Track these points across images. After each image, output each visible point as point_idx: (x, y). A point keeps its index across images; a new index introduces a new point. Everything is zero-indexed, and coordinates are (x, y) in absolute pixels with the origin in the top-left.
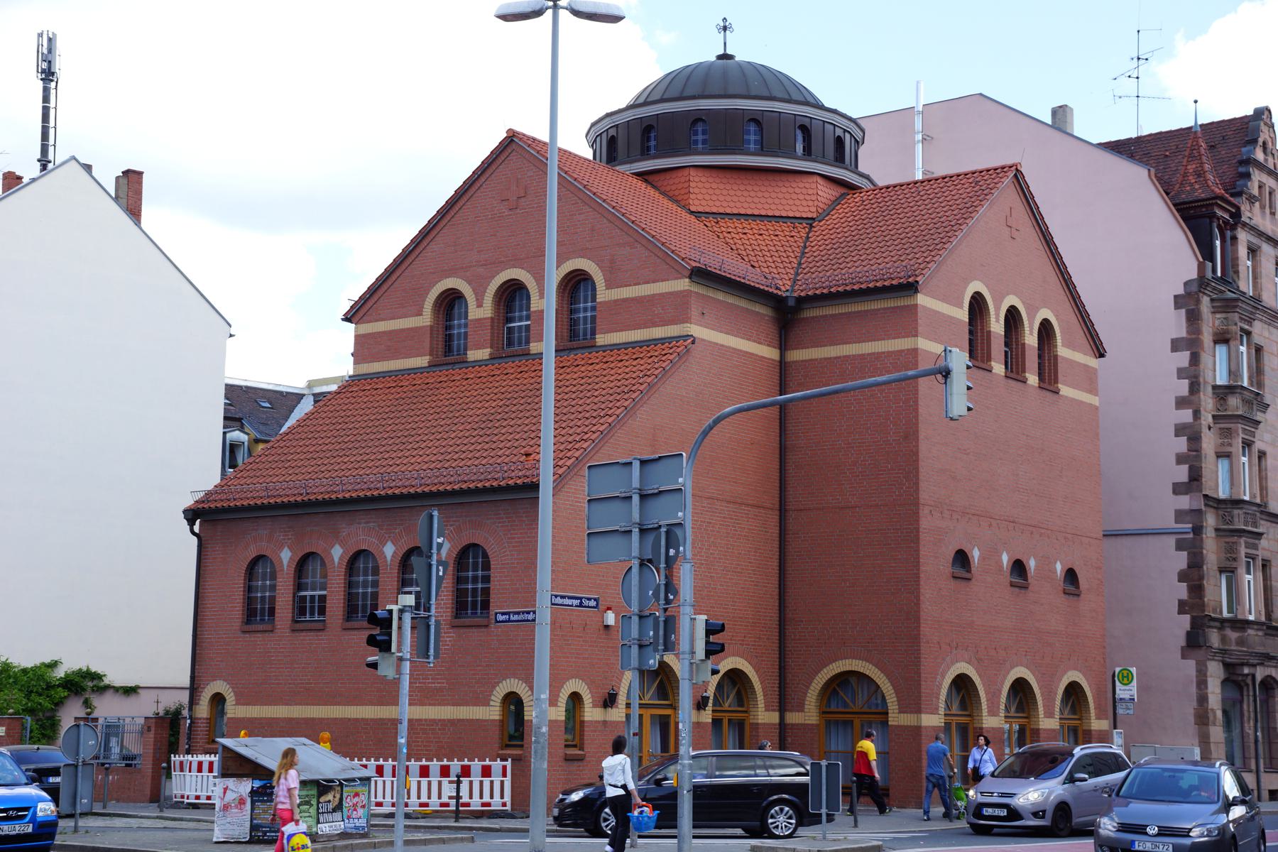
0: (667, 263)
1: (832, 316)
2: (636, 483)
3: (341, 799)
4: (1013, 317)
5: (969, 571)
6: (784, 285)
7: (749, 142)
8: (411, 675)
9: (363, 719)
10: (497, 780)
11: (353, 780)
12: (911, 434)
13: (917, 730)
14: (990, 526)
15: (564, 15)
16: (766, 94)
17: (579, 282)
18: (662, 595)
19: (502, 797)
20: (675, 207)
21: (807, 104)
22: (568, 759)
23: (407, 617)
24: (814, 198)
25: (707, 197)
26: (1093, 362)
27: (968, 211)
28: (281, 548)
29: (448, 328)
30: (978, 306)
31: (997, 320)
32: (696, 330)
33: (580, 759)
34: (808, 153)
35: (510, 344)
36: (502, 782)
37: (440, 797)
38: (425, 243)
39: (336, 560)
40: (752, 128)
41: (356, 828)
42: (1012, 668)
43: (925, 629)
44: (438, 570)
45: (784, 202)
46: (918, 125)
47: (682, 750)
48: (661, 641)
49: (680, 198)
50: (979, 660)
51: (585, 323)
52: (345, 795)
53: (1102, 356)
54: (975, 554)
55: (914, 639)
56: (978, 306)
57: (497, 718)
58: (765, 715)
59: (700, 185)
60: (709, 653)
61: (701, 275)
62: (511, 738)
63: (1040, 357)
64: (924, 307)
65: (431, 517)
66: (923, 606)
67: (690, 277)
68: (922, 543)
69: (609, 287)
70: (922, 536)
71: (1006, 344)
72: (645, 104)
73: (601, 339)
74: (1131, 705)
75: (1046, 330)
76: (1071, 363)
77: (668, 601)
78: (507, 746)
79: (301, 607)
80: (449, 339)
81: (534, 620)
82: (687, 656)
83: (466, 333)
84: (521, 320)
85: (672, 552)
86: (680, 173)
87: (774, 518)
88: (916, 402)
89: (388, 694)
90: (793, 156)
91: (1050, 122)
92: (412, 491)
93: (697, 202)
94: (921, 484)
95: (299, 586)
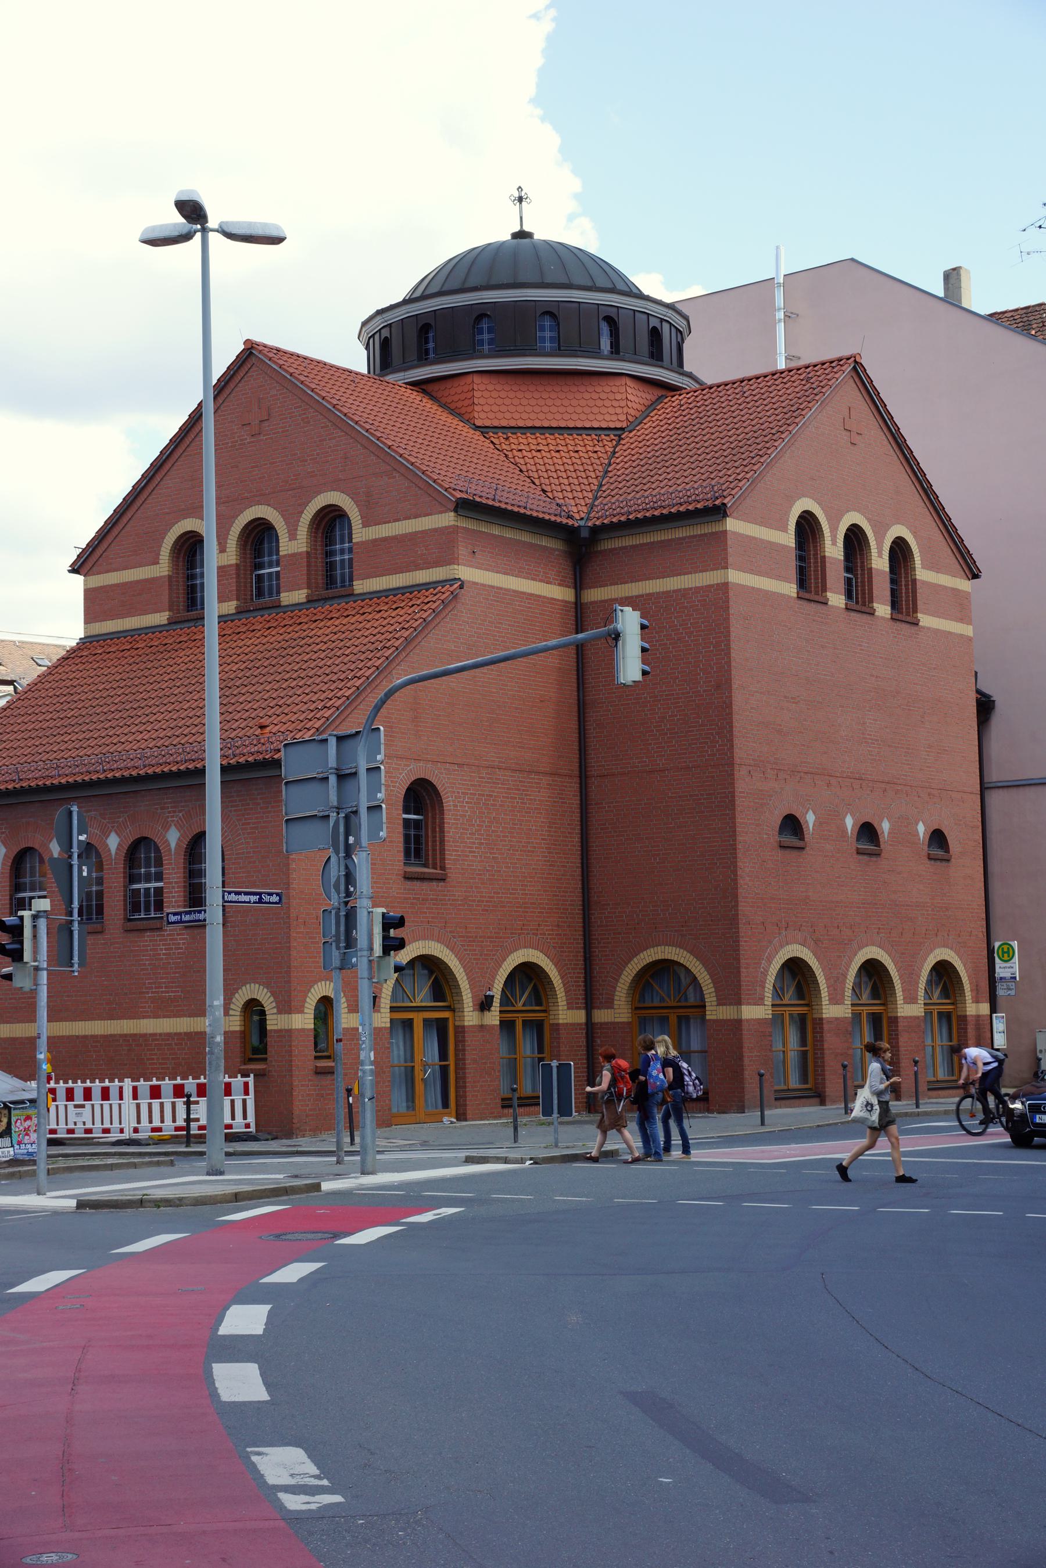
0: (427, 493)
1: (633, 547)
2: (332, 762)
3: (9, 1124)
4: (855, 539)
5: (802, 839)
6: (578, 511)
7: (543, 339)
8: (49, 984)
9: (92, 1036)
10: (238, 1099)
11: (22, 1102)
12: (723, 684)
13: (737, 1024)
14: (829, 785)
15: (214, 238)
16: (564, 280)
17: (334, 519)
18: (342, 887)
19: (245, 1117)
20: (455, 422)
21: (613, 290)
22: (319, 1072)
23: (42, 923)
24: (623, 403)
25: (495, 408)
26: (964, 585)
27: (794, 414)
28: (166, 828)
29: (329, 554)
30: (808, 529)
31: (834, 543)
32: (465, 572)
33: (330, 1072)
34: (616, 351)
35: (260, 593)
36: (244, 1101)
37: (174, 1121)
38: (158, 478)
39: (173, 845)
40: (547, 322)
41: (29, 1154)
42: (860, 948)
43: (745, 908)
44: (80, 871)
45: (587, 410)
46: (779, 300)
47: (363, 1055)
48: (342, 938)
49: (463, 411)
50: (817, 942)
51: (343, 568)
52: (13, 1119)
53: (975, 576)
54: (810, 819)
55: (732, 920)
56: (808, 529)
57: (238, 1028)
58: (566, 1014)
59: (486, 394)
60: (387, 950)
61: (467, 507)
62: (255, 1050)
63: (893, 581)
64: (735, 533)
65: (70, 813)
66: (741, 882)
67: (455, 510)
68: (738, 809)
69: (365, 525)
70: (738, 801)
71: (848, 570)
72: (423, 297)
73: (360, 586)
74: (1012, 985)
75: (900, 552)
76: (936, 588)
77: (348, 894)
78: (251, 1060)
79: (134, 903)
80: (330, 567)
81: (205, 920)
82: (365, 953)
83: (351, 560)
84: (270, 566)
85: (351, 840)
86: (462, 381)
87: (574, 786)
88: (728, 645)
89: (26, 1010)
90: (597, 354)
91: (941, 294)
92: (134, 773)
93: (483, 415)
94: (736, 741)
95: (133, 879)
